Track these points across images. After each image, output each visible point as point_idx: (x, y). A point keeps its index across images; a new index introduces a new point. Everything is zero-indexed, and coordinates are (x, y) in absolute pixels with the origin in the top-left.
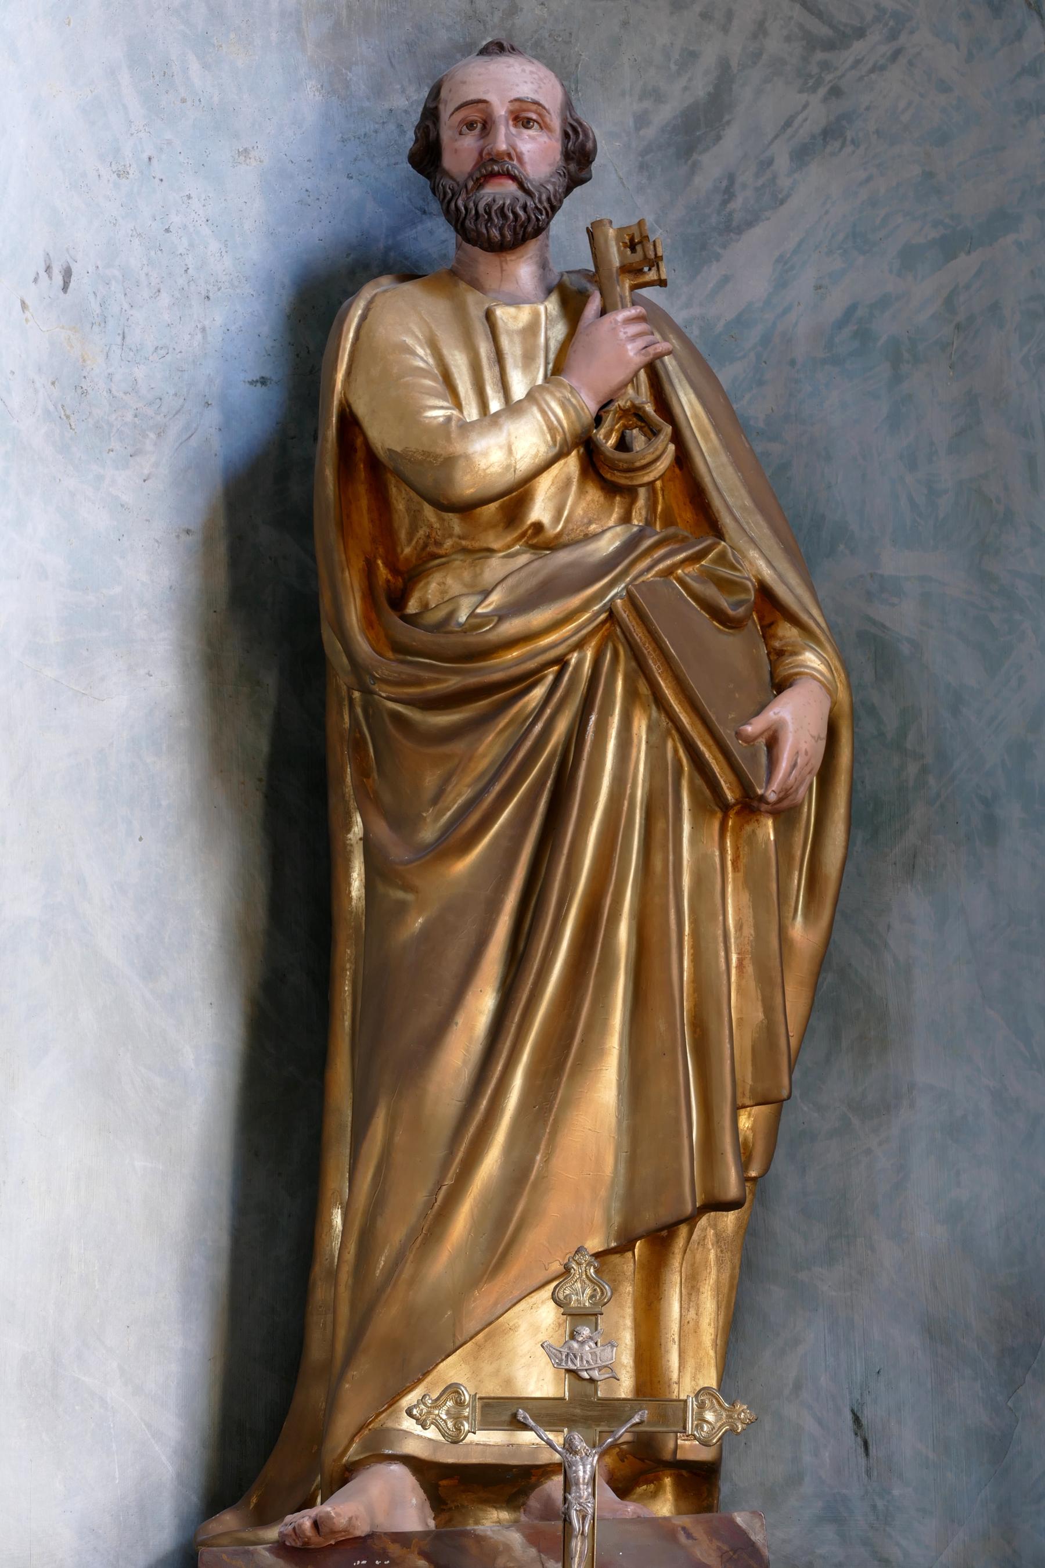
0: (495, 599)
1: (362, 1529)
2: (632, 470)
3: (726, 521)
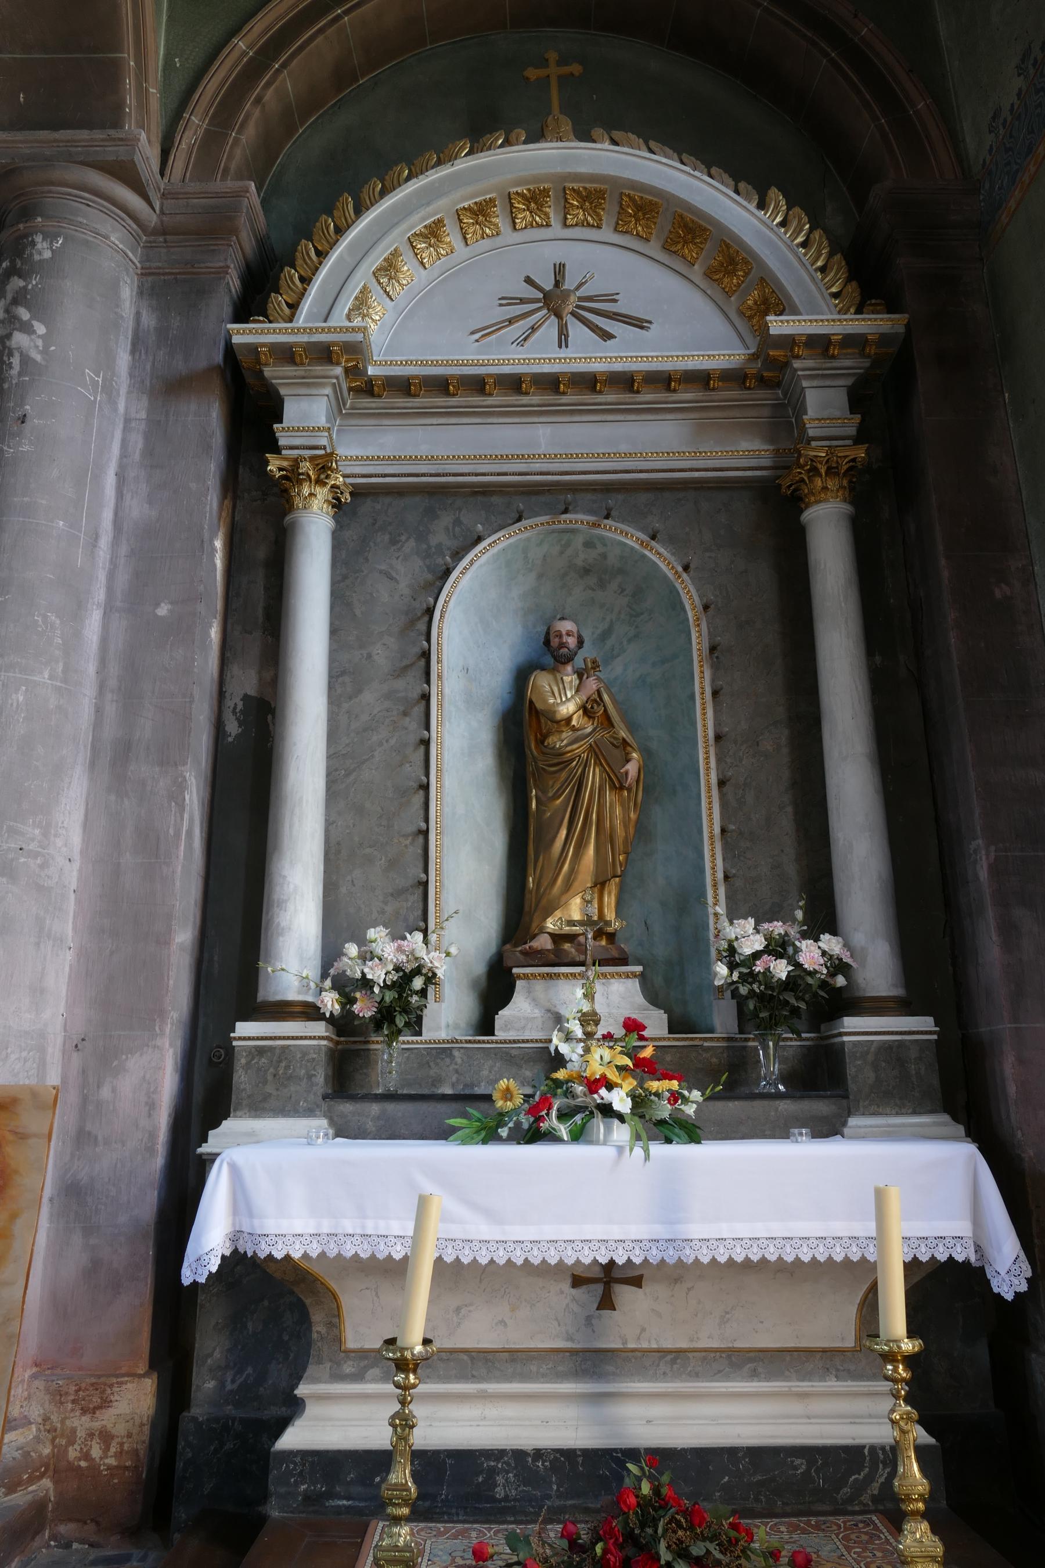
0: (565, 742)
1: (539, 949)
2: (595, 713)
3: (615, 724)
